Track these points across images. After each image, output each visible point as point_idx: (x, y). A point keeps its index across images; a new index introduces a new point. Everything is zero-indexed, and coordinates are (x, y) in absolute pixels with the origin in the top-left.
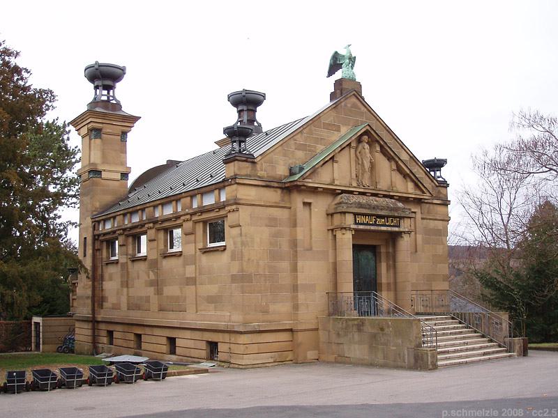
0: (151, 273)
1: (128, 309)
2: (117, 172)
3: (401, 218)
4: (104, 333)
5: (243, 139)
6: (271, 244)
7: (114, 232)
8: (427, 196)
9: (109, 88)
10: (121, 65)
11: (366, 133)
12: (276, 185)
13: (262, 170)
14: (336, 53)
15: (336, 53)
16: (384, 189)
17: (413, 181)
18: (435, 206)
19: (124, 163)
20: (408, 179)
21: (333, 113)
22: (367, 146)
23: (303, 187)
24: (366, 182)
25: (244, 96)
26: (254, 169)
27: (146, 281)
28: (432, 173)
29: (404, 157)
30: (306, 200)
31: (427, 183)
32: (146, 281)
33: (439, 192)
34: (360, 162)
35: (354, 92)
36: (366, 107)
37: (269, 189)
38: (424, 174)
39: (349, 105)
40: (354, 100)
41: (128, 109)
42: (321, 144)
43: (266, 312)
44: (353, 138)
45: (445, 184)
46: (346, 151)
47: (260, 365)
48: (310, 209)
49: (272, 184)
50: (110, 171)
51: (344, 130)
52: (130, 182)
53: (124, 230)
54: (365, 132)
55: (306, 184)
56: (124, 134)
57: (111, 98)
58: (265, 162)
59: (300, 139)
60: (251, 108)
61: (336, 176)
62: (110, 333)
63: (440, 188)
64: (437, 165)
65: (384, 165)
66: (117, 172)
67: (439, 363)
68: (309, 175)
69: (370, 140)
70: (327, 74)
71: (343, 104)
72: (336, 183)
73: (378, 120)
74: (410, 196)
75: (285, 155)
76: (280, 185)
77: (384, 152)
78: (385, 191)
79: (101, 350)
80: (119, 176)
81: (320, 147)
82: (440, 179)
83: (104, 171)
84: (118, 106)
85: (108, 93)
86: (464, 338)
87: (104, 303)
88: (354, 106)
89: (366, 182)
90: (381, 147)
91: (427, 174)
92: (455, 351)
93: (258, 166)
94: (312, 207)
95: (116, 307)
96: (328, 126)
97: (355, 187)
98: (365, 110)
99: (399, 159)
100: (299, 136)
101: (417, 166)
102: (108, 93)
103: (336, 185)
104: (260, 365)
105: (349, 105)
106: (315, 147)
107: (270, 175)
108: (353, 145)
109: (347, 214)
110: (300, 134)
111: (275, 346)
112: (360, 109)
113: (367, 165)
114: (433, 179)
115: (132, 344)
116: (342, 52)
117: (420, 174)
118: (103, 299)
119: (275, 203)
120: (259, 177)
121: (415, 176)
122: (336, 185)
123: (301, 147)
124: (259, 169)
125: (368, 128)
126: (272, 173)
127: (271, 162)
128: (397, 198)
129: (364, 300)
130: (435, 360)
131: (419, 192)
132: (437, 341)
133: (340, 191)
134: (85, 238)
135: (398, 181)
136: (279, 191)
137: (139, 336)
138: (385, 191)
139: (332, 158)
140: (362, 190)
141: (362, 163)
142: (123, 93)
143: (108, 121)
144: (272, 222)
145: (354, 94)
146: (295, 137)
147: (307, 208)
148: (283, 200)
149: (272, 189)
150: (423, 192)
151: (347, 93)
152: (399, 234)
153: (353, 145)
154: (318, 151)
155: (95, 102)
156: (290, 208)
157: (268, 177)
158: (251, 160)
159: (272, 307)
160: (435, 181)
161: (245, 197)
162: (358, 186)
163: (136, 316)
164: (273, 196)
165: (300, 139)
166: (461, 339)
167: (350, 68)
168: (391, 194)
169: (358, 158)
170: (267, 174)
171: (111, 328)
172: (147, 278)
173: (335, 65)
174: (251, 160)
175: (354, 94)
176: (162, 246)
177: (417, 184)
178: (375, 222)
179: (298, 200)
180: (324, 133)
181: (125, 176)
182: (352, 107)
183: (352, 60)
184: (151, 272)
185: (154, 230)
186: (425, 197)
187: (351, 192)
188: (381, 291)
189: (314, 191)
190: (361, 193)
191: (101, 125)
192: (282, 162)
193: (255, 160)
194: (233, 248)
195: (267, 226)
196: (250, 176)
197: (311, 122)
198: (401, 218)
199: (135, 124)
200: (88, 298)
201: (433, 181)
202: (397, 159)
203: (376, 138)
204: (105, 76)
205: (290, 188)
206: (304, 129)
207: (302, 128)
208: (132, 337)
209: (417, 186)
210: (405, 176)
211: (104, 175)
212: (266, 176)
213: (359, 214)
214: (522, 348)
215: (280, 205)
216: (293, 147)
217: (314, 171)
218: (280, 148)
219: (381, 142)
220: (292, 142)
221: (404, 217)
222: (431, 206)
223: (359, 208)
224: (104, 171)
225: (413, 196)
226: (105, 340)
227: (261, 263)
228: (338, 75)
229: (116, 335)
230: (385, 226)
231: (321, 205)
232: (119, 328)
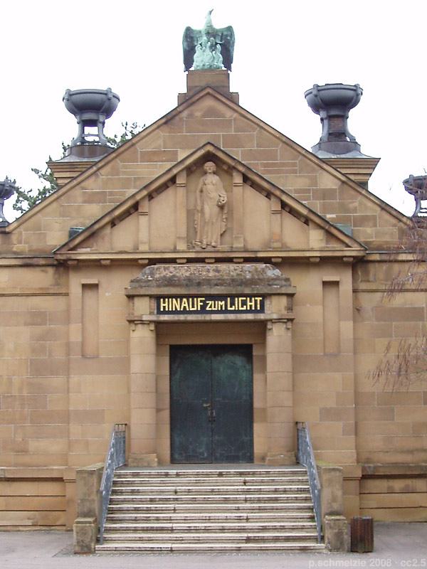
3: (264, 296)
6: (33, 351)
12: (42, 262)
13: (20, 242)
14: (188, 29)
15: (188, 29)
23: (70, 263)
25: (316, 96)
30: (327, 278)
37: (32, 269)
38: (379, 209)
39: (198, 114)
43: (25, 451)
47: (9, 528)
49: (34, 261)
55: (73, 257)
60: (333, 113)
72: (143, 248)
73: (262, 128)
76: (50, 262)
92: (189, 530)
93: (14, 238)
97: (183, 252)
98: (235, 115)
104: (9, 528)
105: (198, 114)
107: (34, 248)
109: (136, 300)
110: (93, 178)
111: (36, 503)
119: (41, 289)
120: (15, 253)
126: (36, 245)
127: (38, 228)
131: (337, 246)
136: (51, 271)
144: (37, 318)
145: (208, 94)
146: (83, 184)
148: (57, 284)
149: (38, 269)
152: (263, 324)
156: (67, 294)
157: (30, 251)
159: (33, 445)
164: (42, 278)
177: (329, 232)
178: (203, 307)
179: (76, 281)
182: (204, 116)
189: (97, 265)
192: (57, 226)
195: (26, 324)
198: (264, 296)
201: (400, 221)
205: (62, 264)
212: (27, 250)
213: (164, 297)
216: (80, 199)
218: (54, 205)
221: (271, 295)
223: (166, 286)
225: (318, 254)
227: (16, 380)
230: (226, 311)
231: (115, 286)
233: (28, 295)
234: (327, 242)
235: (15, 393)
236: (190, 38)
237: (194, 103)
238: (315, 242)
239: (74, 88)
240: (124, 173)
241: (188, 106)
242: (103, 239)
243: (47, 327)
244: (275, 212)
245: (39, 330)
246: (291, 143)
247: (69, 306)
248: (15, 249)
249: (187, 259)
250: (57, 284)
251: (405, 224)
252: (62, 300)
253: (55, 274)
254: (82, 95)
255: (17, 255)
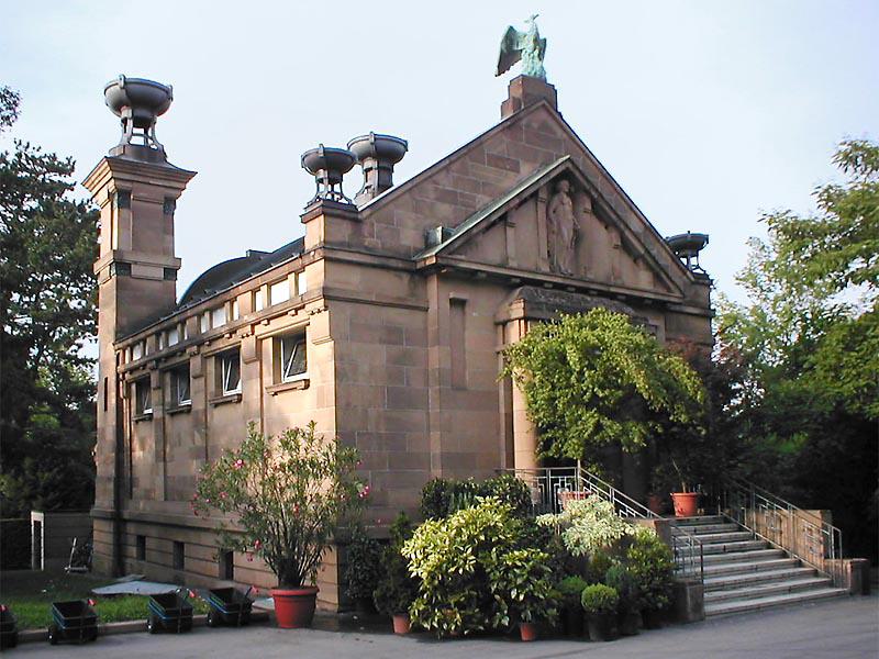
0: (197, 435)
1: (165, 499)
2: (158, 266)
4: (132, 540)
5: (337, 176)
7: (144, 366)
8: (675, 297)
9: (145, 123)
10: (165, 83)
11: (566, 174)
14: (511, 27)
16: (601, 279)
17: (650, 268)
18: (690, 317)
19: (169, 251)
20: (641, 263)
21: (506, 139)
22: (567, 200)
24: (565, 264)
26: (357, 232)
27: (191, 449)
28: (684, 260)
29: (636, 226)
31: (673, 271)
32: (191, 449)
33: (696, 294)
34: (555, 229)
35: (544, 102)
36: (565, 130)
40: (543, 115)
41: (175, 159)
42: (484, 193)
44: (542, 183)
45: (705, 281)
46: (529, 208)
48: (464, 313)
50: (145, 264)
51: (525, 169)
52: (183, 285)
53: (158, 360)
54: (563, 171)
55: (453, 263)
56: (170, 204)
57: (150, 141)
58: (378, 221)
59: (446, 182)
61: (511, 251)
62: (141, 540)
63: (698, 287)
64: (694, 243)
65: (601, 239)
66: (158, 266)
67: (709, 608)
68: (459, 247)
69: (573, 190)
70: (495, 69)
71: (524, 122)
72: (512, 264)
74: (646, 295)
75: (417, 210)
76: (407, 265)
77: (597, 211)
78: (601, 284)
79: (129, 569)
80: (160, 273)
81: (482, 199)
82: (698, 271)
83: (136, 263)
84: (160, 154)
85: (146, 132)
86: (750, 558)
87: (134, 489)
88: (544, 126)
89: (565, 264)
90: (594, 203)
91: (676, 260)
93: (366, 229)
94: (467, 309)
95: (148, 496)
96: (497, 161)
98: (565, 136)
99: (627, 226)
100: (443, 174)
101: (658, 245)
102: (146, 132)
103: (511, 268)
105: (535, 125)
106: (474, 198)
107: (388, 245)
108: (543, 195)
110: (444, 173)
112: (554, 133)
113: (567, 234)
114: (685, 269)
115: (170, 560)
116: (522, 28)
117: (665, 259)
118: (132, 482)
119: (399, 298)
120: (366, 248)
121: (657, 262)
122: (511, 268)
123: (445, 196)
124: (366, 234)
125: (569, 165)
127: (389, 221)
128: (623, 298)
129: (563, 483)
130: (698, 606)
131: (661, 290)
132: (702, 563)
133: (518, 281)
134: (106, 379)
135: (624, 263)
136: (406, 278)
137: (180, 546)
138: (601, 284)
139: (503, 218)
140: (560, 281)
141: (560, 229)
142: (168, 131)
143: (148, 180)
144: (392, 335)
145: (544, 105)
146: (434, 178)
147: (457, 311)
148: (413, 295)
150: (669, 289)
151: (534, 105)
153: (543, 195)
154: (478, 206)
155: (127, 146)
158: (352, 215)
160: (688, 273)
161: (337, 285)
162: (552, 273)
163: (176, 510)
164: (393, 285)
165: (446, 182)
166: (745, 559)
167: (537, 60)
168: (612, 290)
169: (551, 222)
170: (383, 244)
171: (143, 530)
172: (192, 445)
173: (507, 58)
174: (352, 215)
175: (544, 105)
176: (212, 387)
177: (658, 274)
180: (489, 173)
181: (171, 273)
182: (539, 128)
183: (540, 45)
184: (196, 433)
185: (199, 358)
186: (672, 300)
187: (540, 284)
188: (442, 455)
189: (470, 278)
190: (556, 286)
191: (128, 185)
192: (410, 223)
193: (360, 217)
194: (320, 384)
195: (381, 341)
196: (349, 245)
197: (465, 151)
199: (187, 185)
200: (109, 479)
202: (622, 226)
203: (581, 185)
204: (142, 102)
206: (451, 163)
207: (448, 162)
208: (170, 547)
209: (657, 278)
210: (636, 258)
211: (135, 270)
214: (860, 578)
215: (410, 303)
216: (432, 196)
217: (469, 240)
218: (407, 196)
219: (593, 193)
220: (430, 186)
222: (682, 317)
224: (136, 263)
225: (652, 296)
226: (133, 551)
227: (372, 412)
228: (517, 70)
229: (150, 543)
232: (153, 531)
233: (385, 305)
234: (655, 286)
235: (371, 428)
236: (511, 37)
237: (532, 112)
238: (642, 281)
239: (130, 75)
240: (474, 175)
241: (529, 114)
242: (477, 245)
243: (404, 346)
244: (616, 247)
245: (395, 349)
246: (434, 170)
247: (426, 321)
248: (366, 244)
249: (599, 291)
250: (413, 295)
251: (688, 277)
252: (419, 315)
253: (410, 280)
254: (145, 87)
255: (370, 252)
